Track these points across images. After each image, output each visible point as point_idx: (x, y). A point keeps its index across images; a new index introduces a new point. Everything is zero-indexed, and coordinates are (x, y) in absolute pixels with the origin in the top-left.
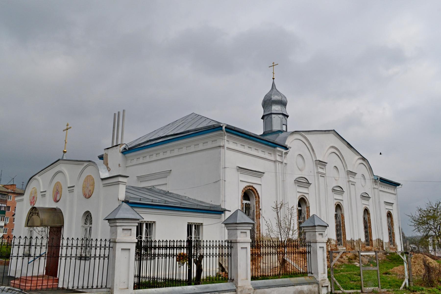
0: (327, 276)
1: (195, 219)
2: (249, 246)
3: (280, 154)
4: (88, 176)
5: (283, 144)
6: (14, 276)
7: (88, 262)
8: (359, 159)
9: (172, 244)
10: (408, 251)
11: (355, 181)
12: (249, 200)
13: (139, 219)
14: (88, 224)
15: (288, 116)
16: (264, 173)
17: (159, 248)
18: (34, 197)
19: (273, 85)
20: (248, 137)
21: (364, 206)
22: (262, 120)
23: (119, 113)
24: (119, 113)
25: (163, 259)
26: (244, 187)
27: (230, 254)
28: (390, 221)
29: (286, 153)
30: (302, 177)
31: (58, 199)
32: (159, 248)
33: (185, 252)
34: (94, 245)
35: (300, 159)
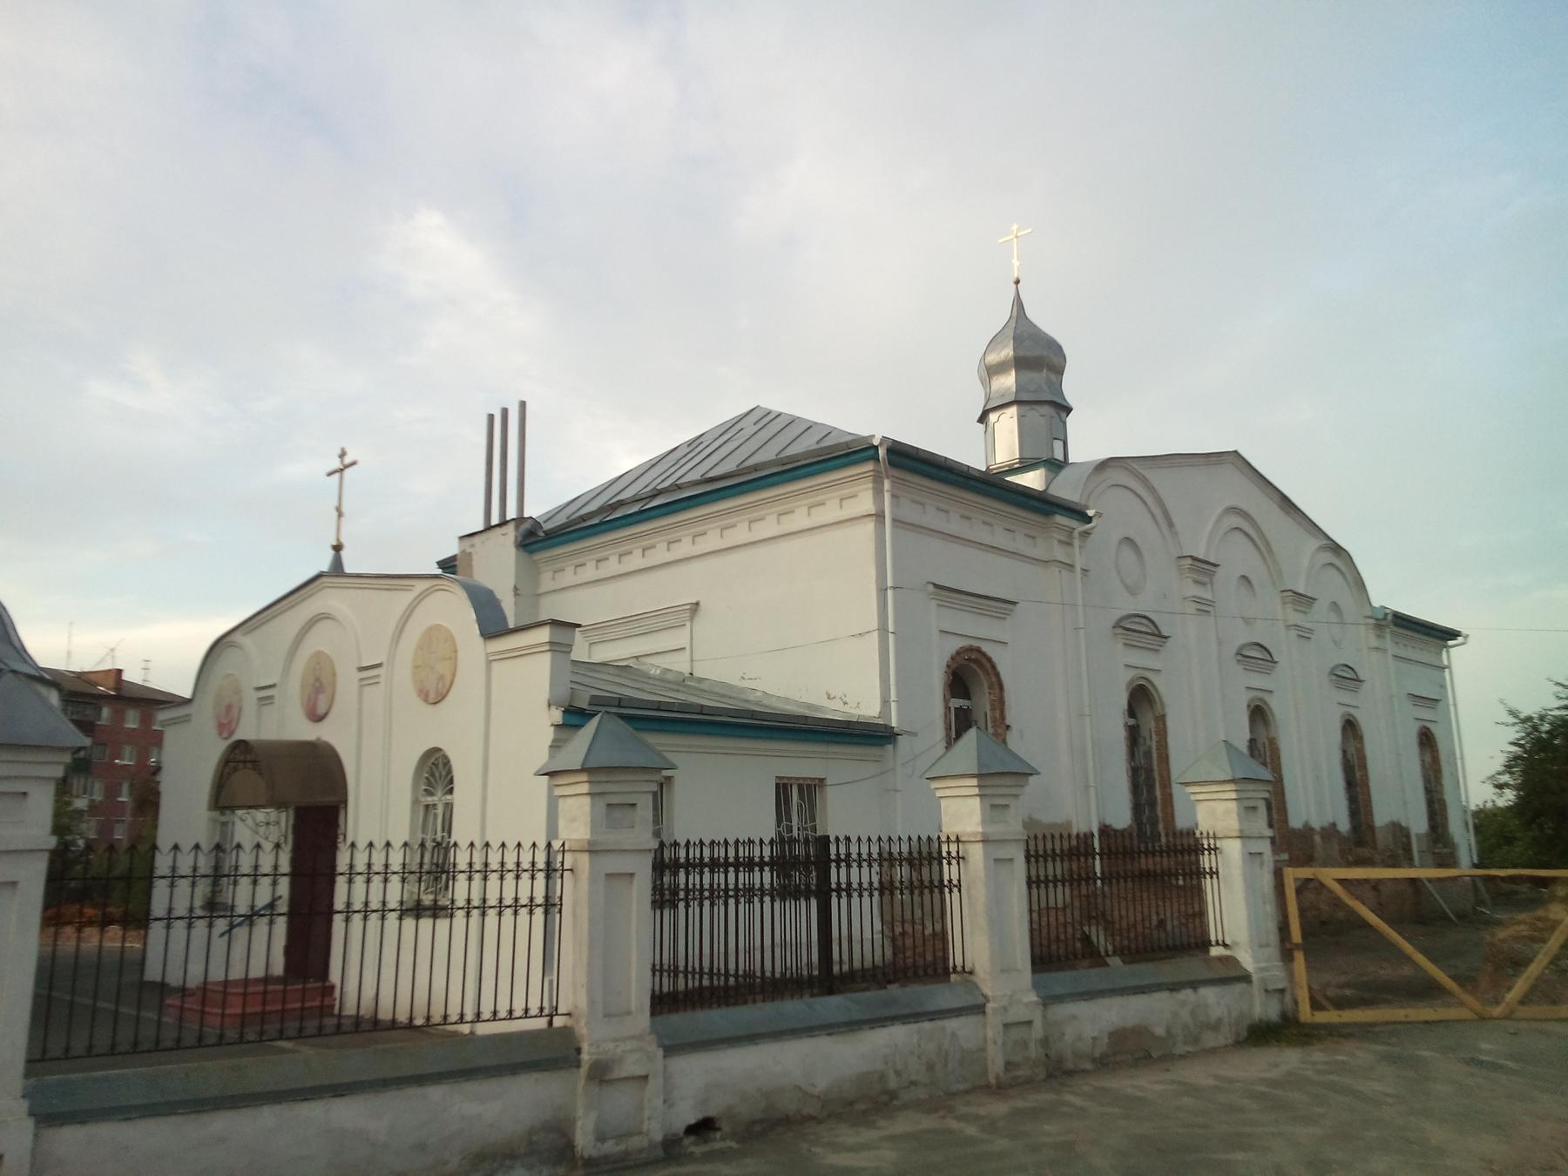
1: (801, 762)
4: (431, 629)
6: (158, 978)
7: (443, 924)
9: (695, 853)
11: (1309, 625)
12: (967, 696)
13: (660, 769)
14: (439, 793)
15: (1068, 410)
16: (1014, 603)
17: (689, 866)
18: (229, 708)
19: (1018, 304)
22: (982, 426)
23: (505, 412)
24: (505, 412)
25: (741, 907)
26: (953, 651)
28: (1428, 759)
29: (1086, 534)
31: (321, 710)
32: (689, 866)
35: (1127, 552)
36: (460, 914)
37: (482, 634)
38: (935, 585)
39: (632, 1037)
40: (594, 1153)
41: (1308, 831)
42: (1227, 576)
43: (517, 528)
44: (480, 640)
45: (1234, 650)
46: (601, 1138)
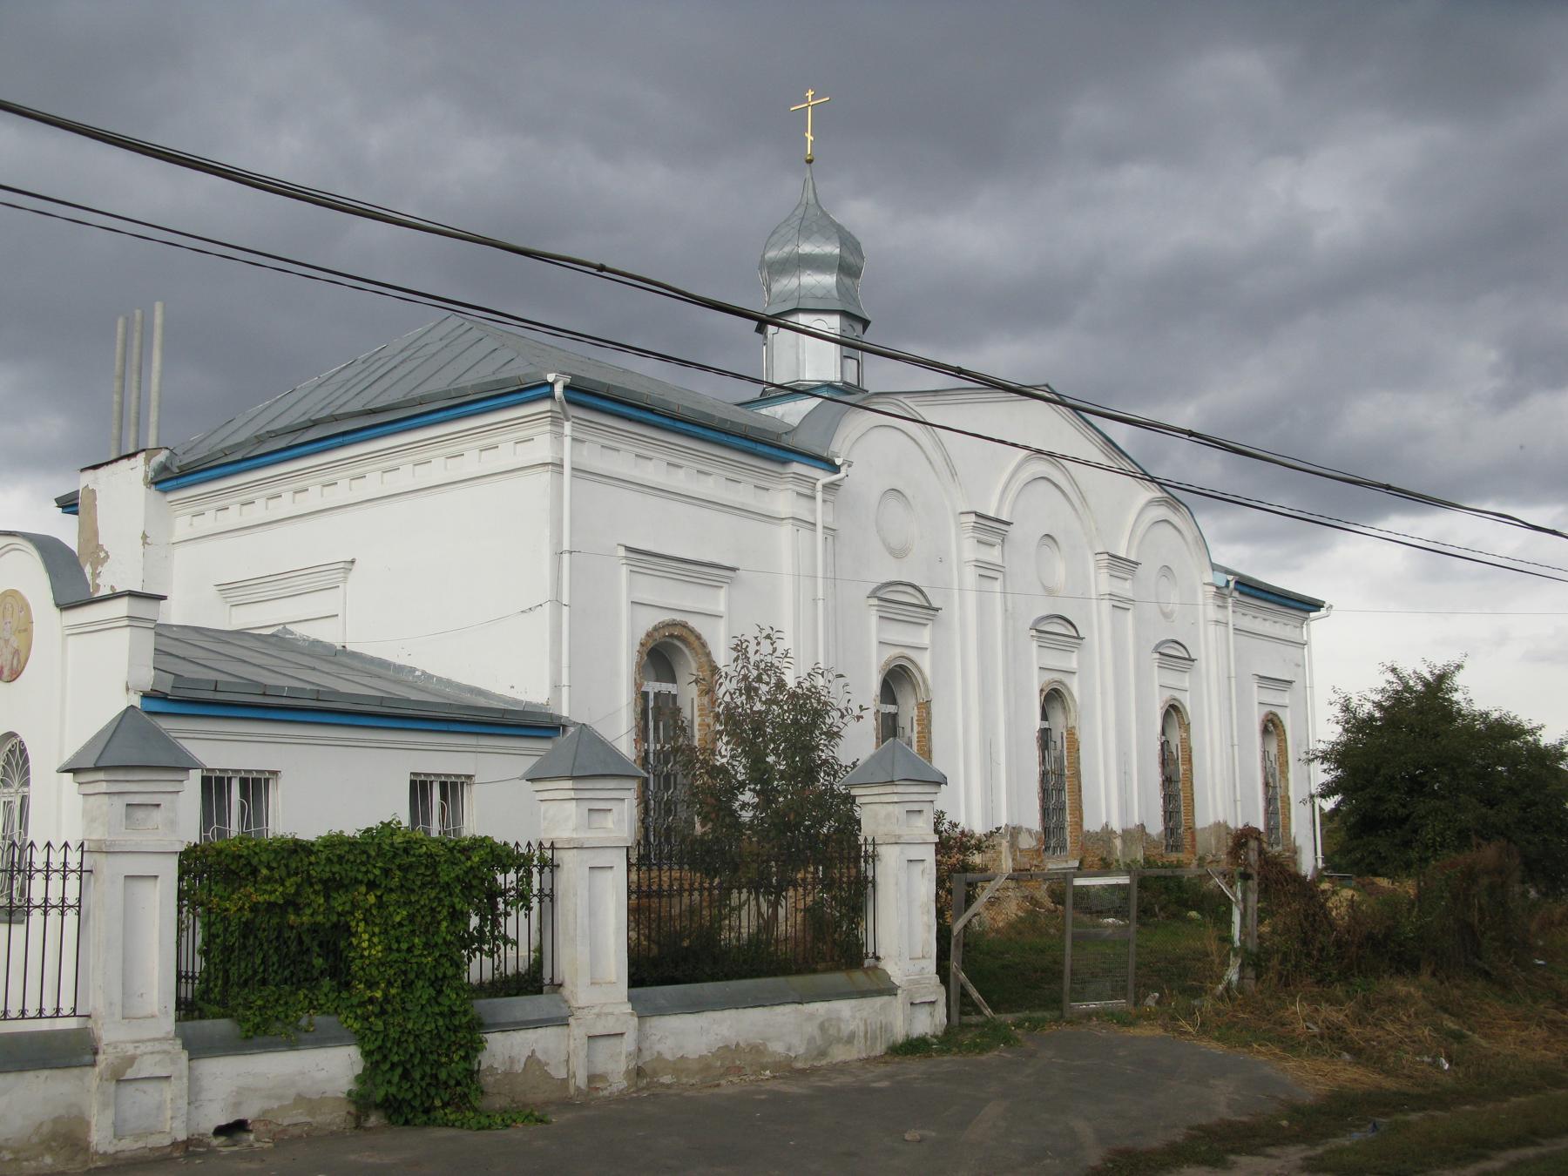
0: (933, 968)
1: (440, 757)
2: (929, 854)
3: (809, 492)
5: (818, 451)
7: (19, 930)
8: (1151, 502)
10: (1250, 871)
12: (673, 680)
20: (340, 440)
21: (1168, 694)
27: (547, 891)
30: (901, 583)
33: (500, 878)
34: (39, 862)
36: (36, 915)
37: (57, 605)
38: (628, 549)
39: (154, 1040)
40: (111, 1150)
41: (1107, 834)
42: (1025, 532)
43: (147, 461)
44: (56, 611)
45: (1030, 623)
46: (118, 1136)
